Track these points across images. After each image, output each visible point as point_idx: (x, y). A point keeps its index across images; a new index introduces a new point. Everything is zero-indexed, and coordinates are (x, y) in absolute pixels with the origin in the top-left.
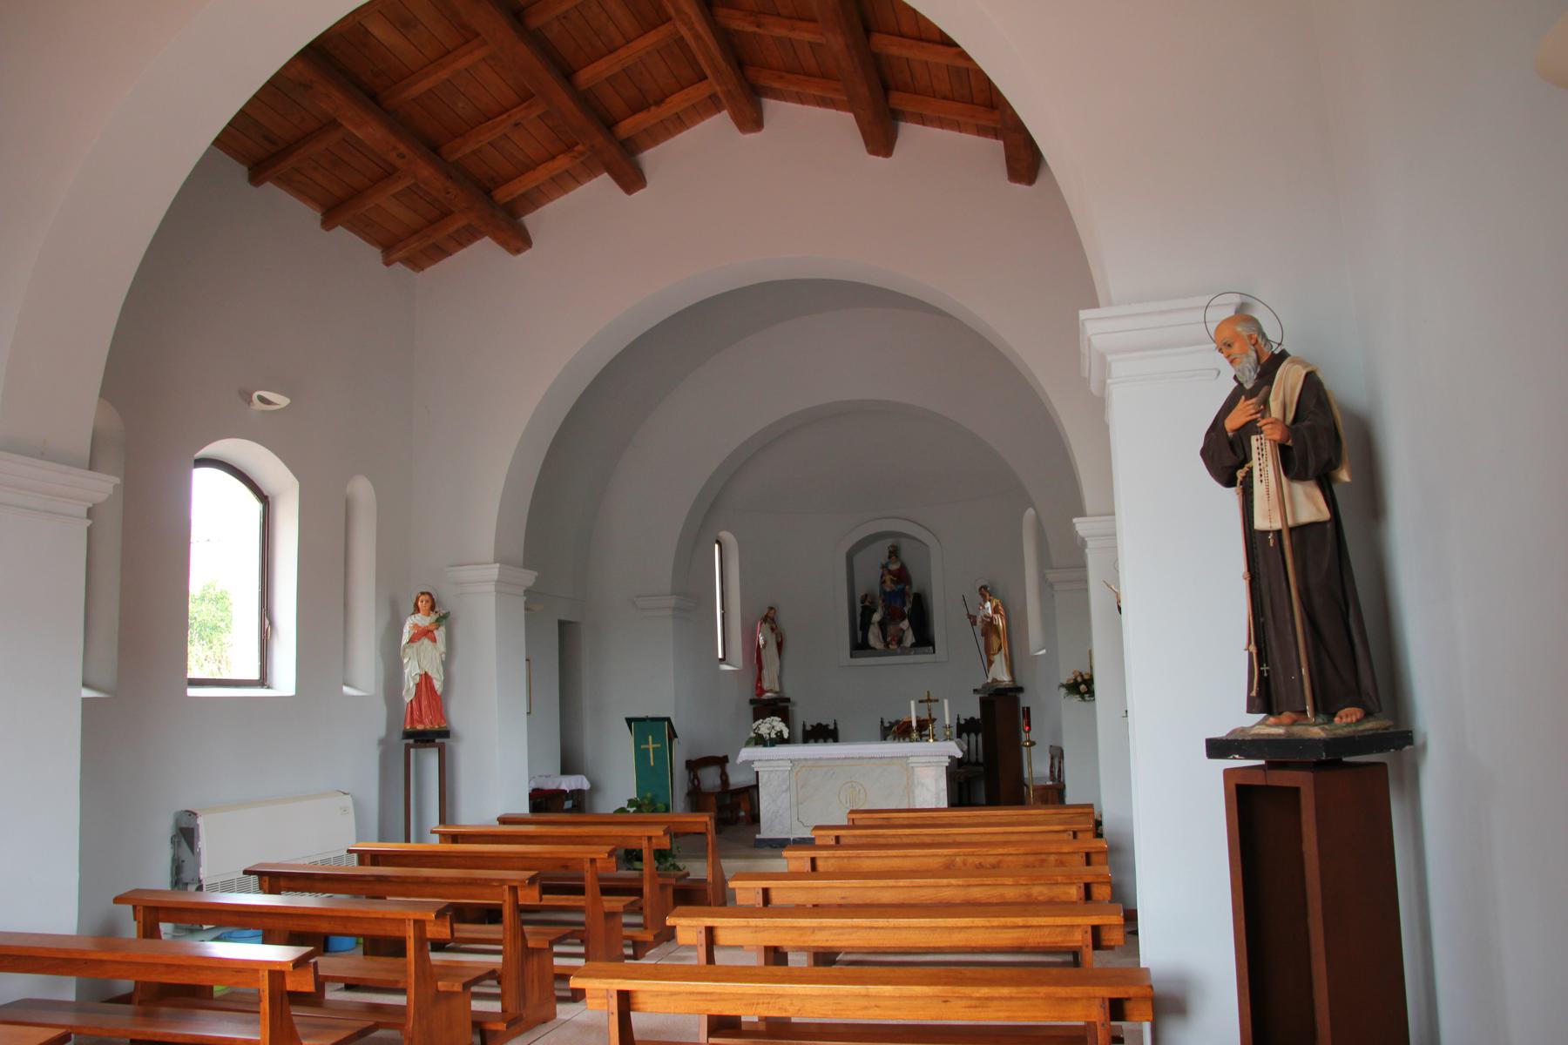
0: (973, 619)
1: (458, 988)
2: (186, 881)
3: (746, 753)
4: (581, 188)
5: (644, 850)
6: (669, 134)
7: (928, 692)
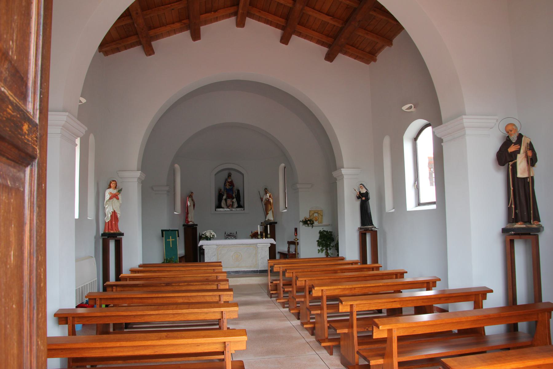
0: (262, 199)
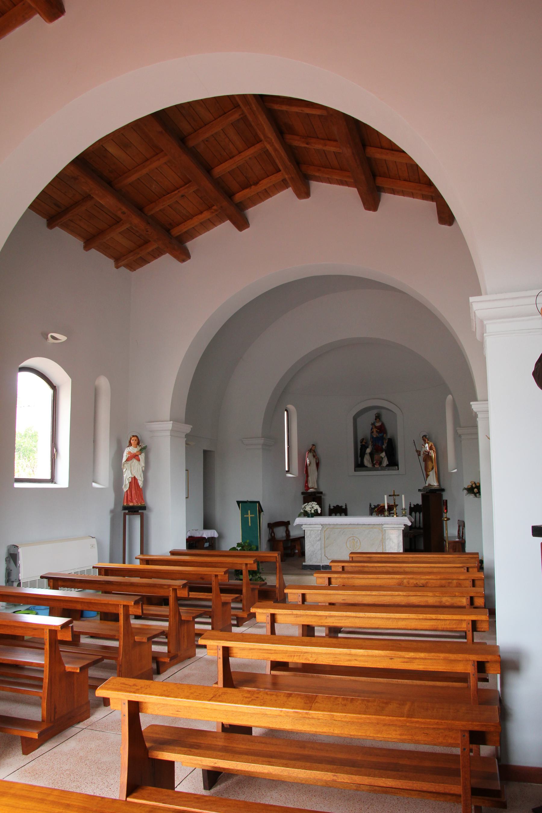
0: (419, 453)
1: (145, 640)
2: (13, 580)
3: (299, 521)
4: (216, 228)
5: (243, 570)
6: (262, 200)
7: (394, 491)
